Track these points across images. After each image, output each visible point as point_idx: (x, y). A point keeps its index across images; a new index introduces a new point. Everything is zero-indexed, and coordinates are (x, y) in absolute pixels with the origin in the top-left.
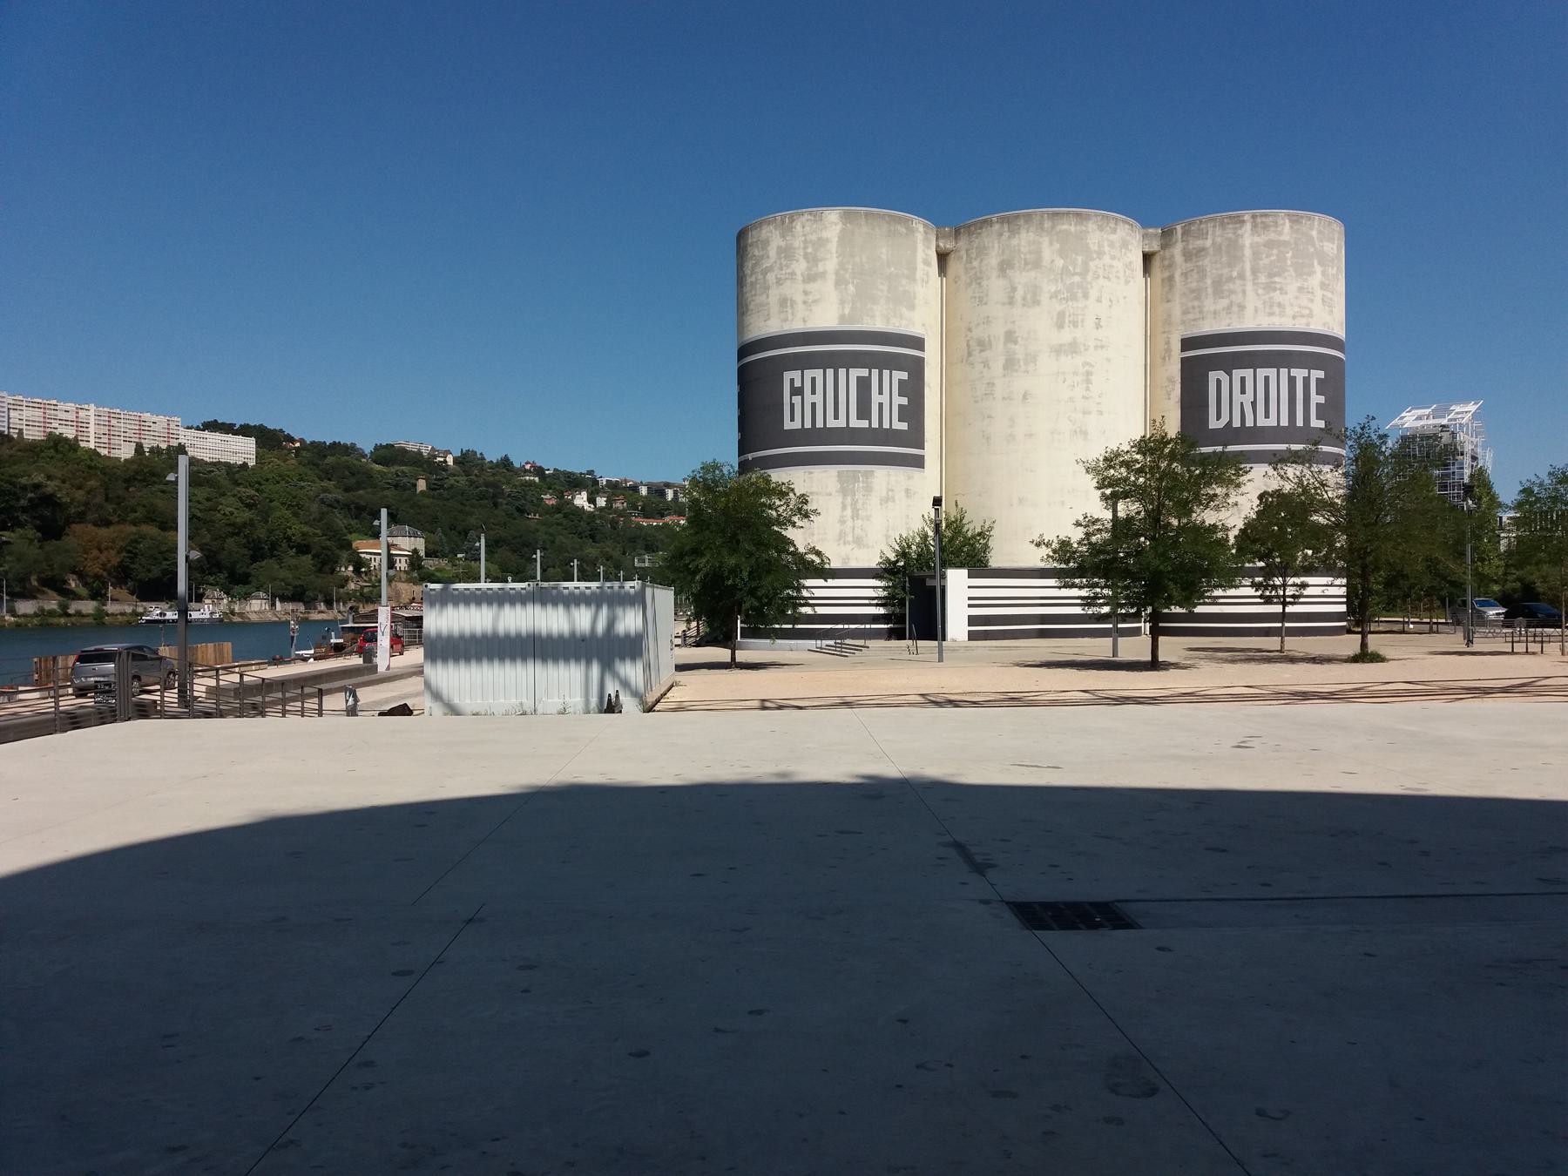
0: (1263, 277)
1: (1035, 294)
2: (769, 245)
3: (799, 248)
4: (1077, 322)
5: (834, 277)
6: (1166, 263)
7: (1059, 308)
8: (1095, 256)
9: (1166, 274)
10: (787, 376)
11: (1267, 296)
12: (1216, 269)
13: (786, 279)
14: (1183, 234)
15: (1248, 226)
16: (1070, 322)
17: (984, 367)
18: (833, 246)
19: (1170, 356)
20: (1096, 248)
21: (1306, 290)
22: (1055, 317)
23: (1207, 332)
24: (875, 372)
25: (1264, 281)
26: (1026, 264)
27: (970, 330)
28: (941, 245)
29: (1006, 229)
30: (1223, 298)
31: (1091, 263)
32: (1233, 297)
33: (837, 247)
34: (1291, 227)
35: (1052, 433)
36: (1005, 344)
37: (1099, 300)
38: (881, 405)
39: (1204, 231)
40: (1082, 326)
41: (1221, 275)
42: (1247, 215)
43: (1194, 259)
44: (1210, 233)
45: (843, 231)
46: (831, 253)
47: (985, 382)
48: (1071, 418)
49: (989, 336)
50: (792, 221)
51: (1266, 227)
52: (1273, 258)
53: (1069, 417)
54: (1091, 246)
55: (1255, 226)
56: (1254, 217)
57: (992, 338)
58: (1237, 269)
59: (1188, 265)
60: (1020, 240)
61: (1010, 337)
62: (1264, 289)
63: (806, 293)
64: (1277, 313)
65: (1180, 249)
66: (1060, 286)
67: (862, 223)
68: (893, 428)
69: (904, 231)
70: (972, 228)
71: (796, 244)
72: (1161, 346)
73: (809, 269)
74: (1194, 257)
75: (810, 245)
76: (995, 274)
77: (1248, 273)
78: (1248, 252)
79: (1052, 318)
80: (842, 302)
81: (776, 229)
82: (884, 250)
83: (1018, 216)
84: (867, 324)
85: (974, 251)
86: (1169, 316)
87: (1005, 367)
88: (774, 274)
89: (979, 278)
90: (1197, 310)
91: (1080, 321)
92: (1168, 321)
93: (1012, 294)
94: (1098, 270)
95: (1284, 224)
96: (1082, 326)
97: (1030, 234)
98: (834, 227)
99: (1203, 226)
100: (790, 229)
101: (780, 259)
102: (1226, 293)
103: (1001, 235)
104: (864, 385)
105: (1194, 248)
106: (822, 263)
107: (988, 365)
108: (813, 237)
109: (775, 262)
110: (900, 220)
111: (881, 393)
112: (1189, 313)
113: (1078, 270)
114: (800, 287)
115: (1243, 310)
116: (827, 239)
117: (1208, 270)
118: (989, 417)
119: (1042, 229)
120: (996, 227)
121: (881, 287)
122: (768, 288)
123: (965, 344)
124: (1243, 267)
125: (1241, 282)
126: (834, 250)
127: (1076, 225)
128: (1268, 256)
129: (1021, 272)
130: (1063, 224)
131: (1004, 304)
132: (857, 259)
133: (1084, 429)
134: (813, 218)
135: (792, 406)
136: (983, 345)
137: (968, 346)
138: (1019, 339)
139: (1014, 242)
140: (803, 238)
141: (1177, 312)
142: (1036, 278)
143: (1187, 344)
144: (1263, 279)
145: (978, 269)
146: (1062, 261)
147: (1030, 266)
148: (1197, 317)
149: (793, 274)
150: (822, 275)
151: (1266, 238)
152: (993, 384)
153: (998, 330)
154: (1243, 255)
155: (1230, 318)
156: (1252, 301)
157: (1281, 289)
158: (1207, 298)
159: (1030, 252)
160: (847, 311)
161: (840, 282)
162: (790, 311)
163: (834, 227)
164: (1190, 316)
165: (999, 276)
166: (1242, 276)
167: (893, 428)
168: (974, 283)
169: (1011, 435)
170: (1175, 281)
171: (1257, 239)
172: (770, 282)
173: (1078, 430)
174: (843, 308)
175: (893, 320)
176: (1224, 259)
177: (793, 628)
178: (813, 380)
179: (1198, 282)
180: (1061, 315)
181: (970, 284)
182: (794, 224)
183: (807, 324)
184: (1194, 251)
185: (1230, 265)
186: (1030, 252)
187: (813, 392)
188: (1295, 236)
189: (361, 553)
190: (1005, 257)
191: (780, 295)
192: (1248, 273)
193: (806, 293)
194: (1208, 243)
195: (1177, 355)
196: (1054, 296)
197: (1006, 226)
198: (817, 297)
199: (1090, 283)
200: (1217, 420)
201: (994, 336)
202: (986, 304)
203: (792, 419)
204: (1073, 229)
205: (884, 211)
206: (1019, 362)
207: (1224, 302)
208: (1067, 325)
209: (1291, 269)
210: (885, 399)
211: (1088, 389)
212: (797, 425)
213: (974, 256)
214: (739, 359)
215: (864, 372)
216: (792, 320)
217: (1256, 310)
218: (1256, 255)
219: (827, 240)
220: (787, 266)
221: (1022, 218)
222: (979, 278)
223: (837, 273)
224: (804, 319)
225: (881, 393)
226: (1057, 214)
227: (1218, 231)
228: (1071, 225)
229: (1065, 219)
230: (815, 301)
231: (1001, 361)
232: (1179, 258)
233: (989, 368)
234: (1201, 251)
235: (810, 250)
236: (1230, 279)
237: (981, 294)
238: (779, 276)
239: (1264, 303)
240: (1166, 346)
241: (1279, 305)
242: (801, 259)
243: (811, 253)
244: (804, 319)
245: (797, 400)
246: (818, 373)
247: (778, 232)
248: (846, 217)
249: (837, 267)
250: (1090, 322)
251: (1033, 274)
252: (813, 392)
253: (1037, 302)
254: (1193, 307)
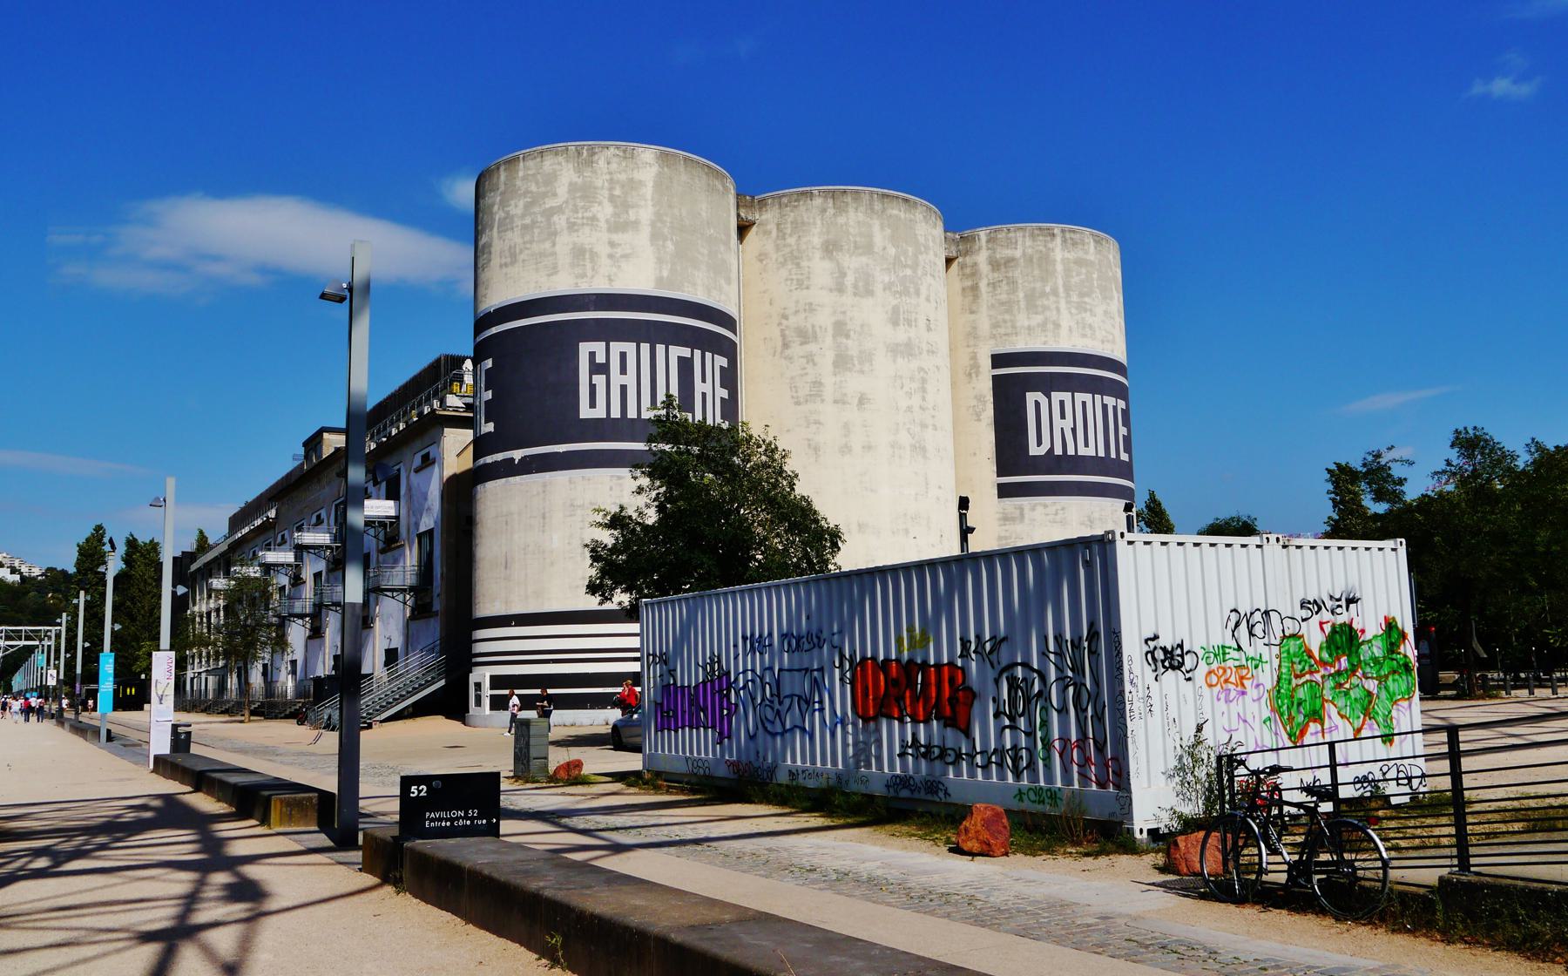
0: (1075, 297)
2: (556, 180)
3: (602, 188)
6: (968, 271)
7: (895, 302)
8: (923, 249)
9: (969, 283)
10: (585, 348)
11: (1079, 316)
13: (583, 224)
14: (988, 241)
15: (1058, 240)
17: (808, 362)
18: (648, 191)
20: (923, 242)
23: (1062, 348)
26: (856, 247)
27: (785, 317)
28: (743, 215)
29: (831, 205)
30: (1036, 313)
31: (920, 257)
32: (1048, 313)
33: (653, 194)
34: (1096, 248)
35: (893, 447)
36: (834, 336)
38: (704, 395)
39: (1014, 241)
40: (916, 326)
41: (1034, 289)
42: (1057, 228)
43: (1003, 269)
44: (1020, 243)
45: (659, 175)
49: (813, 326)
51: (1075, 244)
52: (1083, 277)
53: (909, 429)
55: (1064, 241)
56: (1063, 231)
57: (818, 330)
58: (1050, 284)
59: (996, 275)
60: (848, 219)
61: (840, 329)
62: (1077, 308)
63: (612, 244)
64: (1089, 335)
65: (985, 257)
68: (1070, 394)
70: (785, 200)
71: (599, 183)
72: (965, 361)
73: (616, 215)
75: (618, 187)
76: (818, 254)
77: (1061, 290)
78: (1059, 267)
79: (887, 313)
80: (660, 261)
82: (704, 206)
84: (689, 292)
85: (789, 225)
86: (975, 328)
87: (836, 364)
88: (563, 218)
89: (796, 258)
90: (1009, 324)
92: (973, 334)
95: (1088, 243)
99: (1012, 235)
100: (590, 163)
101: (574, 198)
102: (1040, 309)
103: (824, 211)
104: (685, 366)
105: (1002, 258)
107: (813, 360)
108: (623, 177)
109: (567, 202)
110: (718, 175)
111: (704, 380)
112: (999, 327)
114: (605, 236)
116: (641, 181)
118: (817, 422)
119: (872, 209)
120: (818, 201)
122: (555, 234)
123: (779, 334)
124: (1055, 283)
126: (649, 197)
129: (850, 256)
131: (831, 290)
132: (676, 211)
134: (621, 154)
135: (593, 388)
136: (806, 336)
137: (783, 336)
138: (852, 333)
139: (841, 220)
141: (984, 325)
143: (998, 360)
144: (1075, 298)
145: (795, 247)
146: (894, 250)
147: (860, 251)
148: (1009, 331)
149: (594, 218)
150: (635, 225)
154: (1055, 271)
155: (1046, 336)
157: (1091, 310)
158: (1019, 312)
160: (665, 274)
161: (656, 236)
162: (589, 266)
164: (1002, 331)
166: (1055, 292)
167: (1070, 394)
168: (789, 263)
169: (846, 446)
170: (980, 291)
171: (1067, 255)
174: (660, 271)
175: (715, 293)
176: (1036, 272)
178: (623, 356)
179: (1008, 294)
180: (896, 310)
181: (783, 264)
182: (596, 157)
184: (1003, 261)
185: (1044, 280)
187: (623, 371)
188: (1098, 256)
192: (1061, 290)
193: (612, 244)
194: (1018, 253)
195: (987, 373)
196: (888, 287)
197: (830, 201)
199: (920, 279)
200: (1038, 446)
202: (808, 288)
203: (593, 404)
204: (902, 215)
206: (852, 360)
207: (1038, 319)
209: (1097, 290)
210: (707, 387)
211: (924, 399)
212: (599, 413)
214: (477, 333)
215: (685, 352)
216: (593, 277)
217: (1070, 330)
218: (1067, 271)
220: (586, 209)
222: (796, 258)
223: (653, 224)
225: (704, 380)
227: (1028, 242)
230: (625, 256)
231: (830, 356)
232: (984, 267)
235: (617, 192)
236: (1043, 294)
239: (1077, 323)
240: (972, 362)
242: (606, 202)
243: (619, 197)
244: (609, 276)
245: (599, 380)
246: (629, 348)
247: (571, 166)
248: (663, 157)
249: (653, 218)
250: (922, 323)
251: (864, 259)
253: (869, 293)
254: (1005, 321)
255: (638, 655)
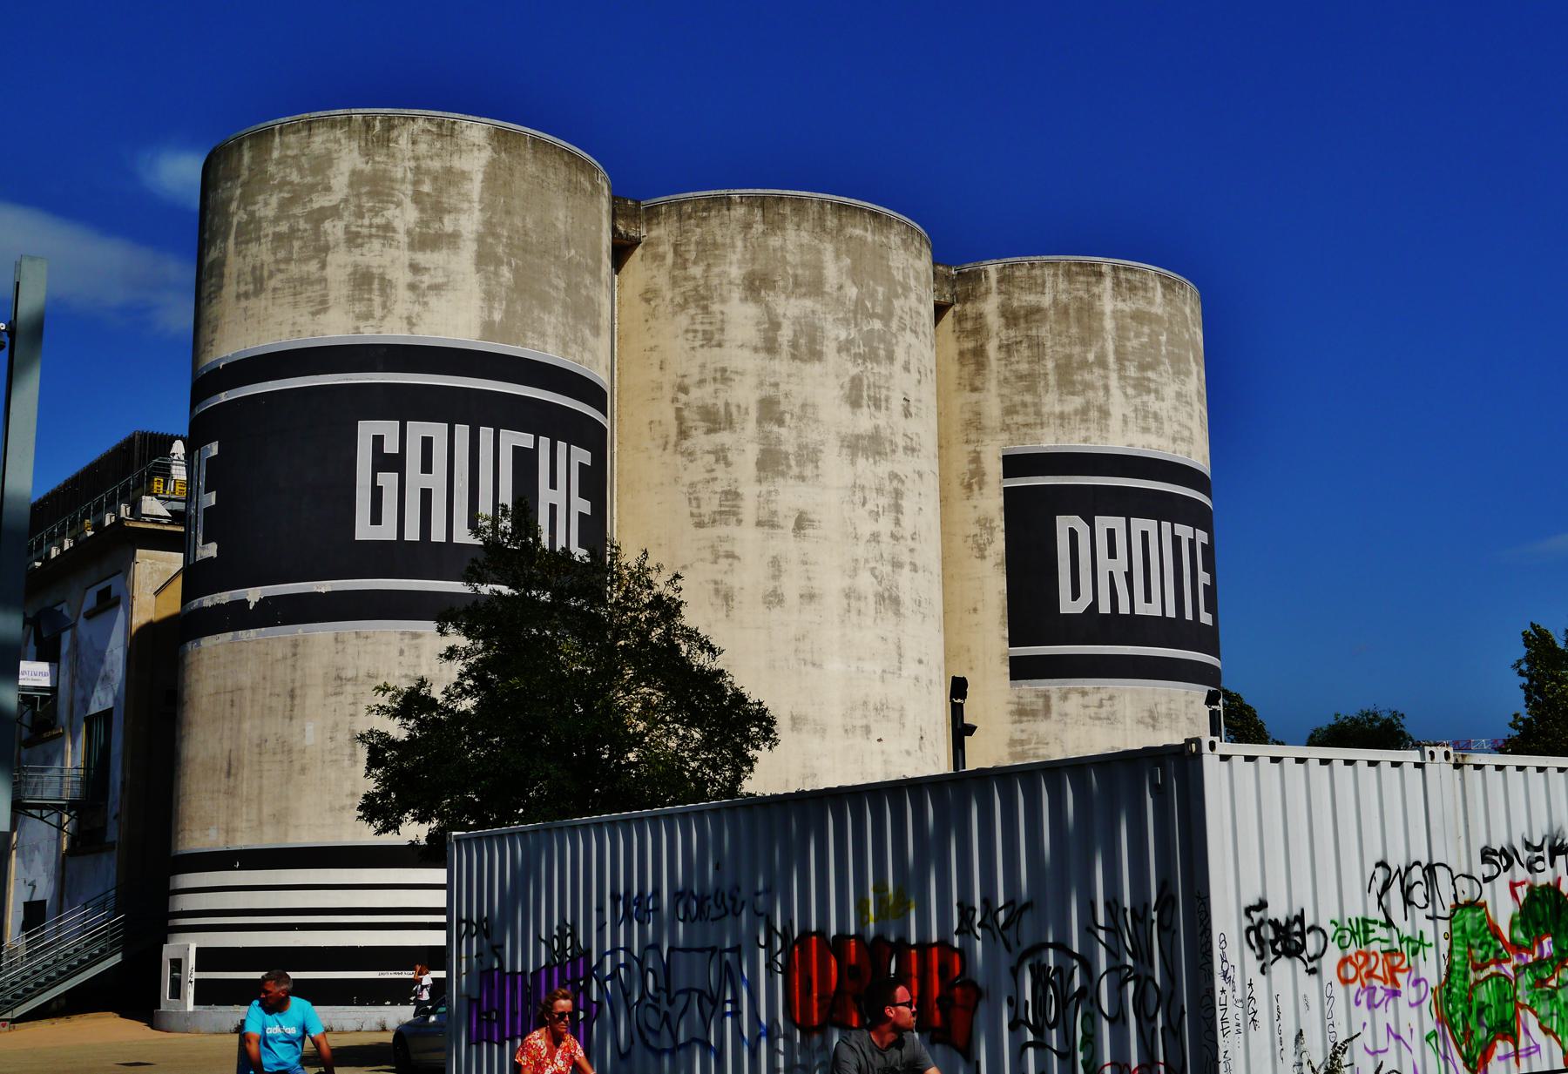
0: (1132, 369)
1: (812, 340)
3: (403, 180)
4: (880, 400)
5: (474, 246)
6: (969, 325)
7: (854, 371)
8: (900, 291)
10: (367, 430)
11: (1138, 400)
12: (1063, 346)
13: (371, 236)
14: (1000, 281)
15: (1108, 282)
16: (869, 396)
17: (717, 461)
18: (475, 187)
19: (981, 485)
21: (1184, 399)
22: (847, 386)
24: (545, 442)
25: (1133, 375)
26: (797, 284)
27: (684, 389)
32: (1090, 394)
33: (482, 192)
34: (1164, 296)
35: (848, 596)
36: (759, 422)
37: (906, 369)
38: (553, 508)
39: (1039, 281)
40: (887, 409)
41: (1069, 357)
43: (1022, 324)
44: (1049, 284)
45: (493, 164)
46: (470, 202)
47: (719, 490)
48: (877, 573)
50: (389, 125)
52: (1145, 339)
53: (873, 570)
54: (895, 273)
55: (1117, 284)
56: (1115, 269)
57: (734, 410)
59: (1012, 333)
61: (769, 410)
62: (1135, 387)
63: (415, 268)
64: (1153, 430)
66: (853, 333)
67: (528, 156)
69: (588, 186)
72: (961, 465)
73: (423, 223)
74: (1022, 321)
75: (427, 181)
76: (736, 294)
77: (1111, 358)
78: (1109, 324)
79: (842, 387)
80: (489, 297)
81: (350, 138)
83: (781, 199)
85: (693, 247)
88: (340, 225)
91: (883, 397)
92: (975, 423)
93: (770, 334)
94: (904, 316)
96: (887, 409)
97: (803, 233)
98: (476, 153)
99: (1037, 272)
100: (385, 141)
101: (358, 195)
102: (1079, 388)
104: (525, 461)
105: (1020, 307)
106: (452, 216)
107: (725, 458)
108: (436, 165)
109: (346, 201)
111: (553, 485)
112: (1017, 413)
113: (879, 310)
114: (405, 256)
115: (1106, 419)
116: (463, 173)
117: (1048, 344)
118: (730, 555)
120: (739, 212)
121: (555, 281)
122: (326, 249)
124: (1102, 347)
125: (1102, 372)
126: (475, 196)
127: (873, 233)
128: (1138, 335)
129: (788, 298)
130: (855, 226)
131: (756, 350)
132: (518, 221)
133: (894, 594)
134: (434, 129)
135: (377, 493)
137: (680, 418)
138: (787, 417)
139: (774, 241)
140: (412, 164)
141: (993, 408)
142: (813, 312)
143: (1014, 464)
144: (1132, 371)
145: (702, 282)
147: (803, 290)
151: (1134, 307)
152: (737, 495)
153: (745, 394)
154: (1102, 329)
155: (1088, 429)
156: (1118, 405)
159: (803, 265)
161: (485, 259)
162: (377, 300)
163: (476, 153)
164: (1019, 419)
165: (746, 299)
166: (1102, 362)
170: (988, 357)
171: (1120, 305)
172: (330, 238)
173: (886, 595)
174: (491, 309)
176: (1074, 330)
177: (784, 1054)
178: (427, 443)
179: (1029, 362)
180: (856, 382)
181: (683, 307)
182: (394, 134)
183: (415, 329)
185: (1085, 342)
186: (803, 265)
187: (427, 467)
189: (1496, 1017)
190: (757, 267)
191: (356, 266)
192: (1111, 358)
193: (415, 268)
194: (1046, 301)
196: (844, 347)
198: (440, 280)
201: (739, 406)
202: (720, 345)
203: (376, 519)
204: (869, 237)
205: (563, 143)
206: (787, 458)
207: (1077, 402)
208: (865, 402)
210: (559, 497)
211: (897, 522)
213: (692, 256)
215: (526, 440)
216: (383, 318)
218: (1121, 330)
219: (464, 176)
221: (788, 203)
222: (703, 298)
223: (480, 239)
224: (409, 319)
225: (553, 485)
226: (848, 207)
228: (867, 230)
229: (858, 218)
230: (436, 288)
231: (752, 452)
232: (994, 320)
233: (728, 464)
234: (1033, 314)
236: (1084, 364)
237: (707, 327)
238: (354, 229)
239: (1136, 410)
240: (973, 466)
241: (1156, 416)
242: (408, 203)
243: (428, 195)
245: (388, 480)
247: (354, 145)
249: (481, 229)
251: (809, 303)
252: (427, 467)
253: (816, 355)
254: (1024, 405)
255: (442, 919)
